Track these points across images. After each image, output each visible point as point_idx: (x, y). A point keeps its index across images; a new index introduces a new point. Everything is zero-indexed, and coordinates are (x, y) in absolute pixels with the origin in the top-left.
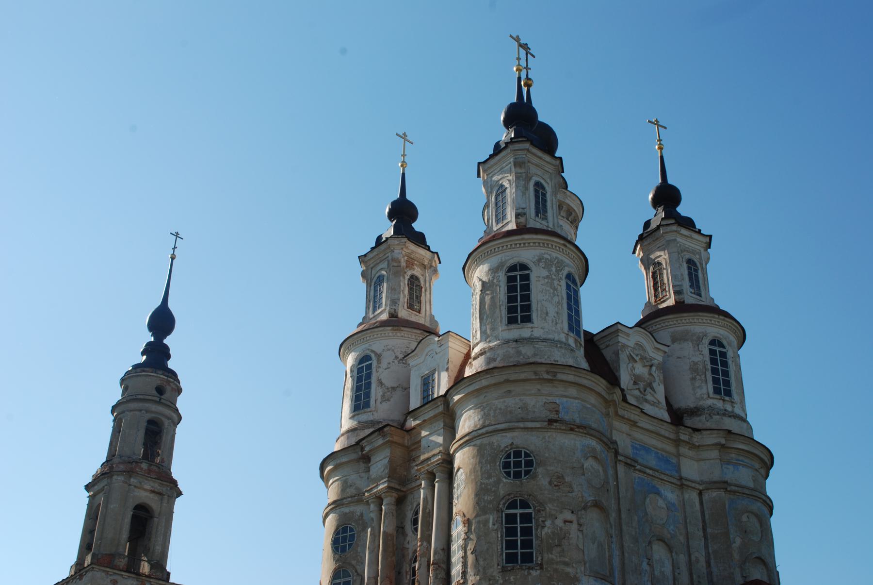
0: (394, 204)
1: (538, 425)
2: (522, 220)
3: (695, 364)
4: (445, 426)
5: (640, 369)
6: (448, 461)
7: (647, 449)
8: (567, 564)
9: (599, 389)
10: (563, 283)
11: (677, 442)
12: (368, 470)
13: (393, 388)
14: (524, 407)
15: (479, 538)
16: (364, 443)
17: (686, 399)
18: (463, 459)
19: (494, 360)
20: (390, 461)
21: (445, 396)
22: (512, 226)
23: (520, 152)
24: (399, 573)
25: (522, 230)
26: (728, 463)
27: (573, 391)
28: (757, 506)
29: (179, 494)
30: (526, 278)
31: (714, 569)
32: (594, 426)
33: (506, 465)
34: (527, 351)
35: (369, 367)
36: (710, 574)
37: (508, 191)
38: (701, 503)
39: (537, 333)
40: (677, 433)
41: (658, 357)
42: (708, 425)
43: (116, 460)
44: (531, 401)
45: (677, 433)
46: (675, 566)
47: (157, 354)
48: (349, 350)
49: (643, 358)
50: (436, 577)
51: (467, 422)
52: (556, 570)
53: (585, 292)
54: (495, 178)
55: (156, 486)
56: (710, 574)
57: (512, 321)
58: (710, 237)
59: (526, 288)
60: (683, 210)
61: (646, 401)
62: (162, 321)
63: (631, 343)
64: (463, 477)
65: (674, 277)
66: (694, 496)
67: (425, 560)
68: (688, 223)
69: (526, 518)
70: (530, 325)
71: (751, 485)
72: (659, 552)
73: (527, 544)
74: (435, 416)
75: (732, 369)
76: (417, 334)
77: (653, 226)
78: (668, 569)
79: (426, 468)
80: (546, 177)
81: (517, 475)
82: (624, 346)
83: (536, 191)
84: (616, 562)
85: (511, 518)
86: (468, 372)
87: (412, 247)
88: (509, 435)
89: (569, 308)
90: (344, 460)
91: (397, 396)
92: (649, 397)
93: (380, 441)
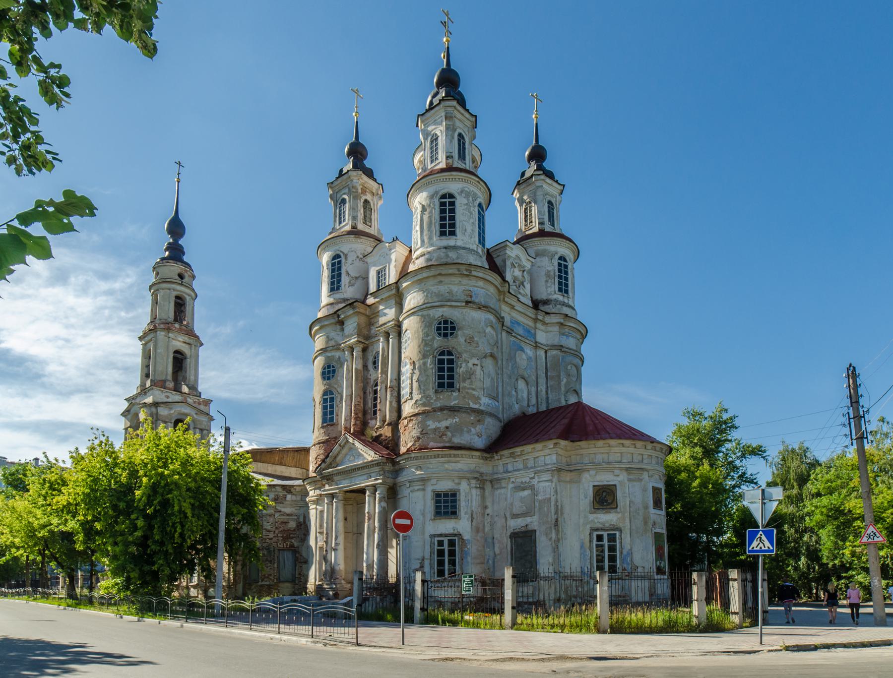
0: (352, 145)
1: (459, 304)
2: (450, 161)
3: (549, 271)
4: (396, 302)
5: (517, 273)
6: (399, 325)
7: (518, 324)
8: (474, 389)
9: (497, 283)
10: (476, 209)
11: (536, 320)
12: (343, 330)
13: (357, 278)
14: (450, 292)
15: (420, 371)
16: (339, 313)
17: (542, 295)
18: (411, 326)
19: (431, 260)
20: (358, 325)
21: (396, 283)
22: (443, 165)
23: (449, 109)
24: (365, 393)
25: (449, 169)
26: (563, 335)
27: (481, 283)
28: (577, 361)
29: (202, 344)
30: (452, 204)
31: (550, 396)
32: (492, 306)
33: (439, 329)
34: (453, 255)
35: (340, 262)
36: (547, 398)
37: (440, 139)
38: (546, 358)
39: (459, 243)
40: (536, 314)
41: (528, 265)
42: (553, 311)
43: (157, 321)
44: (455, 289)
45: (536, 314)
46: (529, 393)
47: (176, 253)
48: (325, 250)
49: (519, 265)
50: (392, 395)
51: (412, 300)
52: (467, 393)
53: (488, 215)
54: (430, 129)
55: (186, 339)
56: (547, 398)
57: (442, 234)
58: (564, 186)
59: (452, 211)
60: (546, 165)
61: (520, 293)
62: (176, 228)
63: (513, 255)
64: (410, 335)
65: (539, 212)
66: (541, 353)
67: (384, 386)
68: (550, 175)
69: (451, 362)
70: (454, 237)
71: (574, 348)
72: (521, 384)
73: (451, 377)
74: (389, 296)
75: (570, 277)
76: (372, 242)
77: (527, 175)
78: (525, 395)
79: (383, 329)
80: (466, 130)
81: (445, 335)
82: (509, 257)
83: (459, 140)
84: (500, 389)
85: (441, 362)
86: (411, 268)
87: (365, 178)
88: (441, 310)
89: (479, 227)
90: (326, 323)
91: (359, 283)
92: (521, 291)
93: (351, 312)
